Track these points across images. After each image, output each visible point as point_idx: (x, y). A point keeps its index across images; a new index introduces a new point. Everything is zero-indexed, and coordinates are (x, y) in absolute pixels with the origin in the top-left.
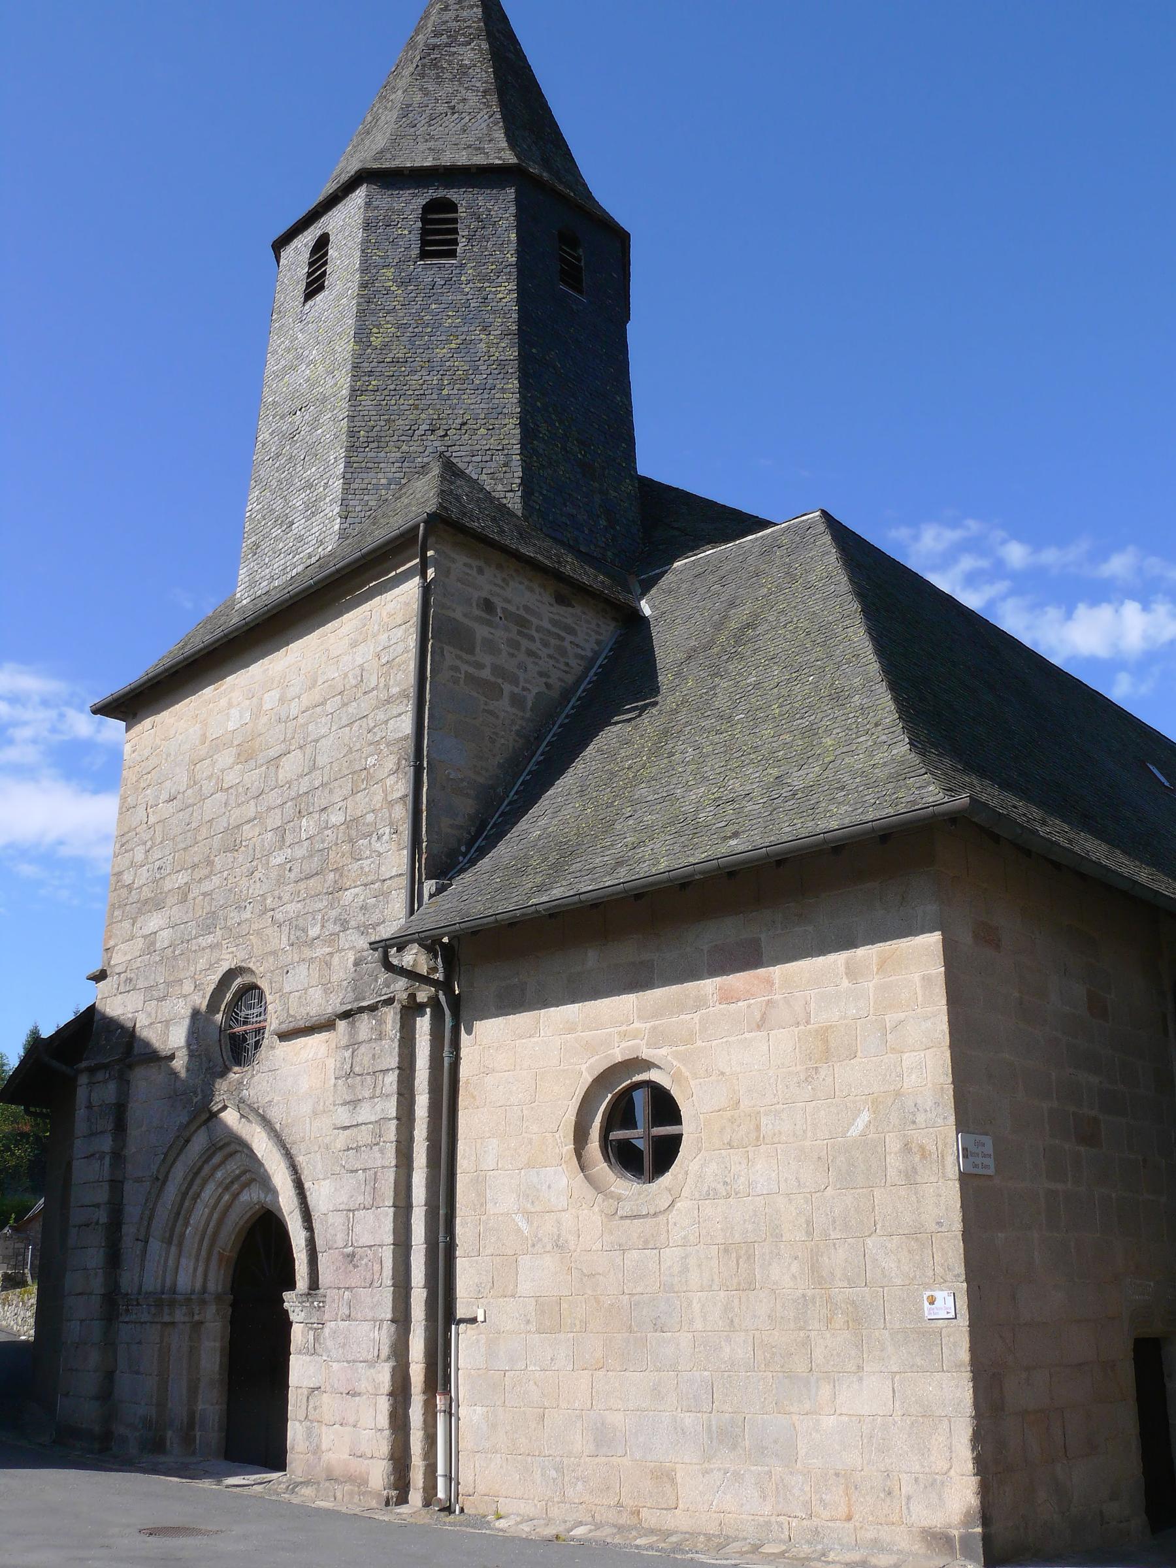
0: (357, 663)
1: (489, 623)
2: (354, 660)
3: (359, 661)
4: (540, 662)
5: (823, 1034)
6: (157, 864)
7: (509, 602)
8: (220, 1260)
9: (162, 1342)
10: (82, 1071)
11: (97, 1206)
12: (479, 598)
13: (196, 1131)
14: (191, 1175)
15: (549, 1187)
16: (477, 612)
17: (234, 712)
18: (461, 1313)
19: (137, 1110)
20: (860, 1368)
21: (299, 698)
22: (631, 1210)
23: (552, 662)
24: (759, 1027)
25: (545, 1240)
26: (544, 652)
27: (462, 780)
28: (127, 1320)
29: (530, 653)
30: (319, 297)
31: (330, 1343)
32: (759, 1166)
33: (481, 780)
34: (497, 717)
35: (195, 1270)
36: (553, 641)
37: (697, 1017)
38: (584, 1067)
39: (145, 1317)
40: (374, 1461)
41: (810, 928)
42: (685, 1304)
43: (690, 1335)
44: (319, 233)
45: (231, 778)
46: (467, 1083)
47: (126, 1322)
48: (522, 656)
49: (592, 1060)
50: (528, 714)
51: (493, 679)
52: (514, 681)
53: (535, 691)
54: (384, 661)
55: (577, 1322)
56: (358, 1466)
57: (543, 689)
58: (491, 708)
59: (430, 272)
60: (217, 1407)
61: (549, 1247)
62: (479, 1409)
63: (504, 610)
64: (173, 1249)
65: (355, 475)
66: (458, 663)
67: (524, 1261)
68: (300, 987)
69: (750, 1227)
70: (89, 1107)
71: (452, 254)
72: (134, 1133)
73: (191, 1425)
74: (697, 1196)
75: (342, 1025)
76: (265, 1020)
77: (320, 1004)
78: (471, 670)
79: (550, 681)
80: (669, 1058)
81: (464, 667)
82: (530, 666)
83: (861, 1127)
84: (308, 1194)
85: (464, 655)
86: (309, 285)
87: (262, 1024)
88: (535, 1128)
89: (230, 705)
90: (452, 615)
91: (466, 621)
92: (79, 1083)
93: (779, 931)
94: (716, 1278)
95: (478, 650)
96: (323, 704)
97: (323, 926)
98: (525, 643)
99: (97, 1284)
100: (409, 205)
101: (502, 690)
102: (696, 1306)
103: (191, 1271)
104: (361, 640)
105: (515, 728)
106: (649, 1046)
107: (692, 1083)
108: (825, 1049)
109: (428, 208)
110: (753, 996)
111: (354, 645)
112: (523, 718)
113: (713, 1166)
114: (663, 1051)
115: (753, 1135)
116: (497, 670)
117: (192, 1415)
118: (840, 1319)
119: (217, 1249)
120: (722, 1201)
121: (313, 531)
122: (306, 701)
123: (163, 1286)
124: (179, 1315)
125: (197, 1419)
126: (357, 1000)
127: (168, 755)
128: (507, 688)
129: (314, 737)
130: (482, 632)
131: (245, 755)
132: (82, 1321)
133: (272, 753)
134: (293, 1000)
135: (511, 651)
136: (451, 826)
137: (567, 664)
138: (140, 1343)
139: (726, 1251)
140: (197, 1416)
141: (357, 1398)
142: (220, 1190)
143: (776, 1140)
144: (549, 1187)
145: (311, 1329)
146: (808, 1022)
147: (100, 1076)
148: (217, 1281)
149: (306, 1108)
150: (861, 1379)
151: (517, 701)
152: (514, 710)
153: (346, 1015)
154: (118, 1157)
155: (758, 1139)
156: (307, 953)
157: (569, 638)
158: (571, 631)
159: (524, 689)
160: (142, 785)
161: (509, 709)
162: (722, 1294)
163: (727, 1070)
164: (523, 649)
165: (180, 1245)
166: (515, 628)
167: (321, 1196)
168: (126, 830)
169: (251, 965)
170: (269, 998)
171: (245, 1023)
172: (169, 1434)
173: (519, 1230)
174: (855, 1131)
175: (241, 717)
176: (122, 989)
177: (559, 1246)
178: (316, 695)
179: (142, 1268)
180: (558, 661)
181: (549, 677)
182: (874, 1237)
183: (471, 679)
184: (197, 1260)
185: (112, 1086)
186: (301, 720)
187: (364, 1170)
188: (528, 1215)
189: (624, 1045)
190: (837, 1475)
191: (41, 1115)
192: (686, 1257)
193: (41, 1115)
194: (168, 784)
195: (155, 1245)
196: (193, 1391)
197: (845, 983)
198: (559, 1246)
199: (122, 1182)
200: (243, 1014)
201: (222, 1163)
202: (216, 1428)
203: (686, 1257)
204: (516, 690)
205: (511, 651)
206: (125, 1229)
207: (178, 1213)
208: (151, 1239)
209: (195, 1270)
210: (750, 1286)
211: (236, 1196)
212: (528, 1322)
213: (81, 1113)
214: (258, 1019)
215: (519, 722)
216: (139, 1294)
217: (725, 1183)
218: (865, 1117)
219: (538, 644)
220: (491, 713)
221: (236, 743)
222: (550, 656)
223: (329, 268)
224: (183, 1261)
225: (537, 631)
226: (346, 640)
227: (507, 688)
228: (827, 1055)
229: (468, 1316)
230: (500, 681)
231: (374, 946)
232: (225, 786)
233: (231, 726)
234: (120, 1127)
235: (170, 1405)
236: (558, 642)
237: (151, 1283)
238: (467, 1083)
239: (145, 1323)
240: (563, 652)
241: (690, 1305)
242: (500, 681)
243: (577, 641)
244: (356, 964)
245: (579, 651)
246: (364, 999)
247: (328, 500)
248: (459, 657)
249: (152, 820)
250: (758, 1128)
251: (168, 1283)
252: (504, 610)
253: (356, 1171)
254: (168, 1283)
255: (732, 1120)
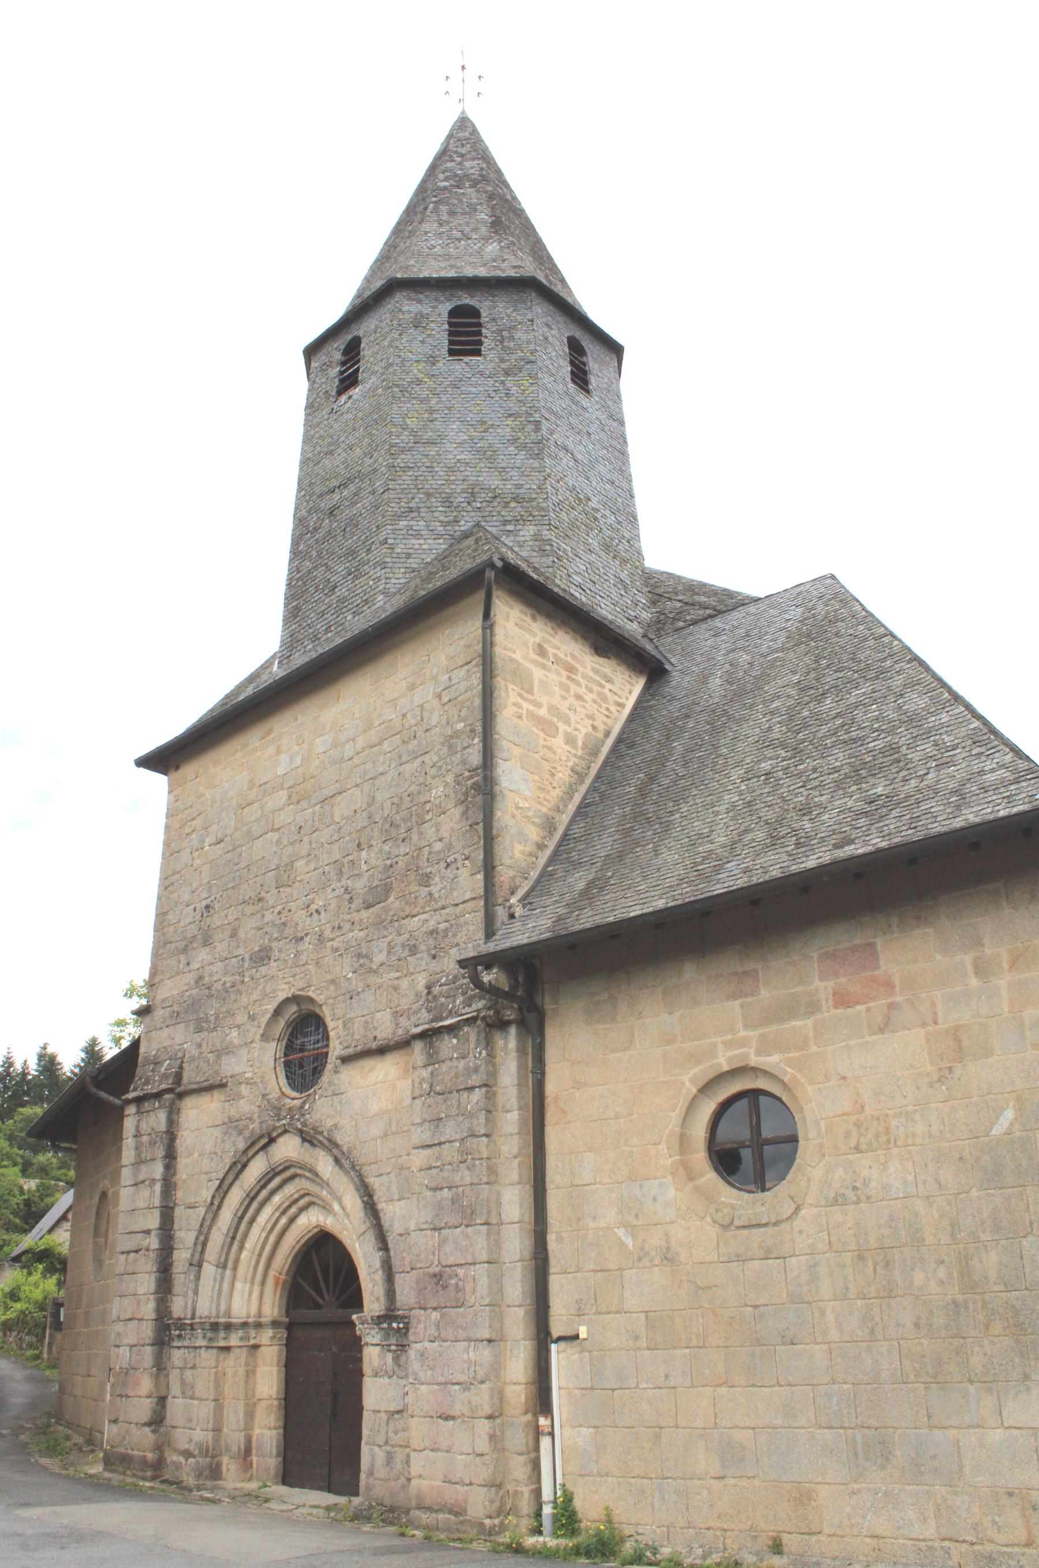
0: (416, 704)
1: (544, 667)
2: (412, 701)
3: (418, 701)
4: (587, 706)
5: (956, 1033)
6: (204, 903)
7: (558, 649)
8: (277, 1284)
9: (216, 1367)
10: (129, 1102)
11: (148, 1232)
12: (534, 643)
13: (253, 1156)
14: (248, 1200)
15: (654, 1199)
16: (534, 656)
17: (284, 758)
18: (557, 1329)
19: (186, 1139)
20: (1026, 1377)
21: (354, 740)
22: (749, 1220)
23: (595, 706)
24: (881, 1031)
25: (653, 1253)
26: (589, 697)
27: (529, 809)
28: (180, 1344)
29: (579, 697)
30: (356, 392)
31: (415, 1366)
32: (892, 1169)
33: (544, 810)
34: (555, 753)
35: (250, 1294)
36: (596, 688)
37: (809, 1022)
38: (686, 1079)
39: (201, 1342)
40: (474, 1487)
41: (931, 930)
42: (816, 1315)
43: (824, 1347)
44: (349, 337)
45: (283, 818)
46: (556, 1098)
47: (179, 1348)
48: (572, 700)
49: (697, 1070)
50: (579, 753)
51: (549, 717)
52: (567, 722)
53: (584, 731)
54: (445, 700)
55: (693, 1337)
56: (453, 1494)
57: (590, 730)
58: (548, 743)
59: (460, 367)
60: (274, 1432)
61: (657, 1261)
62: (585, 1431)
63: (555, 655)
64: (228, 1272)
65: (398, 541)
66: (520, 700)
67: (630, 1274)
68: (366, 1012)
69: (887, 1232)
70: (137, 1135)
71: (478, 353)
72: (183, 1163)
73: (248, 1451)
74: (823, 1202)
75: (418, 1046)
76: (327, 1046)
77: (385, 1028)
78: (531, 708)
79: (596, 723)
80: (782, 1065)
81: (525, 705)
82: (579, 709)
83: (1006, 1125)
84: (381, 1214)
85: (525, 695)
86: (342, 381)
87: (325, 1050)
88: (635, 1141)
89: (279, 752)
90: (514, 656)
91: (527, 665)
92: (127, 1112)
93: (896, 935)
94: (851, 1286)
95: (536, 690)
96: (380, 744)
97: (389, 953)
98: (573, 687)
99: (149, 1309)
100: (438, 311)
101: (557, 729)
102: (830, 1316)
103: (246, 1294)
104: (419, 682)
105: (570, 764)
106: (759, 1053)
107: (809, 1088)
108: (957, 1048)
109: (452, 313)
110: (873, 999)
111: (412, 687)
112: (575, 756)
113: (840, 1171)
114: (775, 1058)
115: (883, 1139)
116: (553, 709)
117: (249, 1441)
118: (997, 1327)
119: (272, 1273)
120: (852, 1207)
121: (358, 592)
122: (361, 742)
123: (218, 1311)
124: (234, 1340)
125: (254, 1445)
126: (435, 1020)
127: (214, 801)
128: (562, 727)
129: (371, 775)
130: (538, 674)
131: (297, 798)
132: (131, 1346)
133: (327, 792)
134: (357, 1026)
135: (564, 693)
136: (523, 853)
137: (608, 709)
138: (193, 1367)
139: (861, 1258)
140: (254, 1440)
141: (451, 1423)
142: (277, 1214)
143: (910, 1142)
144: (654, 1199)
145: (389, 1351)
146: (936, 1023)
147: (147, 1105)
148: (272, 1307)
149: (376, 1130)
150: (1028, 1389)
151: (570, 740)
152: (568, 748)
153: (423, 1035)
154: (169, 1186)
155: (888, 1141)
156: (372, 979)
157: (608, 686)
158: (609, 681)
159: (576, 729)
160: (187, 830)
161: (563, 746)
162: (859, 1302)
163: (849, 1074)
164: (572, 693)
165: (235, 1269)
166: (564, 673)
167: (396, 1213)
168: (170, 873)
169: (311, 994)
170: (330, 1024)
171: (302, 1050)
172: (225, 1460)
173: (622, 1245)
174: (997, 1130)
175: (291, 762)
176: (169, 1022)
177: (669, 1258)
178: (373, 736)
179: (196, 1292)
180: (600, 706)
181: (594, 720)
182: (1030, 1238)
183: (531, 715)
184: (252, 1283)
185: (162, 1116)
186: (356, 761)
187: (450, 1188)
188: (632, 1230)
189: (730, 1053)
190: (1010, 1494)
191: (69, 1150)
192: (814, 1266)
193: (69, 1150)
194: (214, 828)
195: (209, 1270)
196: (250, 1414)
197: (974, 982)
198: (669, 1258)
199: (173, 1208)
200: (299, 1042)
201: (280, 1187)
202: (274, 1452)
203: (814, 1266)
204: (569, 730)
205: (564, 693)
206: (176, 1255)
207: (233, 1238)
208: (205, 1264)
209: (250, 1294)
210: (889, 1293)
211: (292, 1220)
212: (637, 1338)
213: (129, 1142)
214: (316, 1046)
215: (573, 759)
216: (193, 1318)
217: (855, 1188)
218: (1009, 1114)
219: (584, 690)
220: (550, 748)
221: (286, 786)
222: (594, 701)
223: (362, 365)
224: (239, 1285)
225: (583, 678)
226: (404, 684)
227: (562, 727)
228: (960, 1053)
229: (568, 1333)
230: (555, 720)
231: (463, 963)
232: (277, 826)
233: (281, 771)
234: (171, 1157)
235: (225, 1430)
236: (600, 689)
237: (205, 1307)
238: (557, 1098)
239: (200, 1347)
240: (605, 699)
241: (823, 1313)
242: (555, 720)
243: (614, 689)
244: (429, 987)
245: (616, 698)
246: (442, 1019)
247: (371, 564)
248: (520, 695)
249: (197, 862)
250: (887, 1130)
251: (223, 1307)
252: (555, 655)
253: (441, 1189)
254: (223, 1307)
255: (857, 1125)
